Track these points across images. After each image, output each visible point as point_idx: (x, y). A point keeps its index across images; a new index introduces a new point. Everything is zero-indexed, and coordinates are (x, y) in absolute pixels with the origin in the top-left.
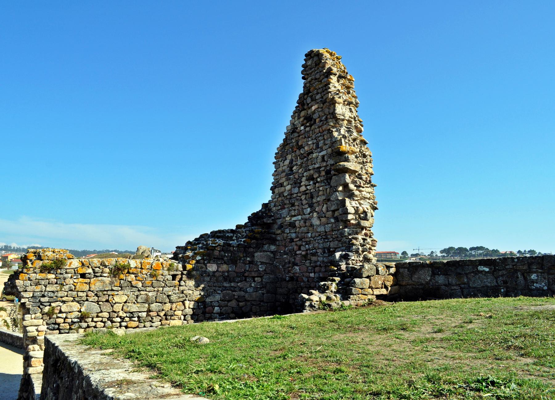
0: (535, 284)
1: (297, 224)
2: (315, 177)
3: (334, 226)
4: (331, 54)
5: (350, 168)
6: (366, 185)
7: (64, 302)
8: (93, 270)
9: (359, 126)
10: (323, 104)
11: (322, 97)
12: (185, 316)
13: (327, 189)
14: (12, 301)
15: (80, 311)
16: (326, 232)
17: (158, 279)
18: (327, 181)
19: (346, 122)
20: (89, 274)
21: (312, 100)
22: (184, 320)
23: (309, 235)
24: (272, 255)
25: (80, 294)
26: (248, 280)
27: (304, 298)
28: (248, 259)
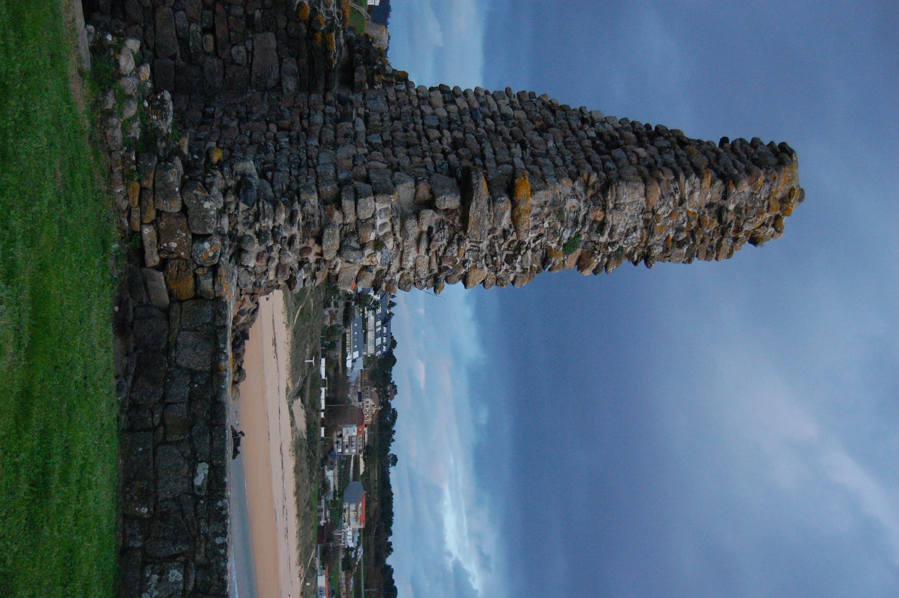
0: (156, 577)
5: (474, 204)
6: (434, 260)
9: (596, 262)
19: (599, 215)
24: (271, 83)
26: (206, 12)
28: (258, 14)
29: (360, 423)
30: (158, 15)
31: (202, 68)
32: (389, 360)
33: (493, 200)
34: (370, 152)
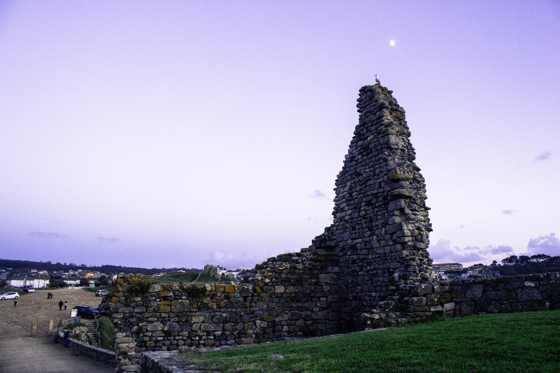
1: (358, 246)
2: (373, 202)
8: (174, 293)
11: (377, 129)
19: (399, 151)
20: (170, 296)
28: (313, 280)
30: (315, 318)
31: (332, 302)
33: (403, 187)
34: (376, 235)
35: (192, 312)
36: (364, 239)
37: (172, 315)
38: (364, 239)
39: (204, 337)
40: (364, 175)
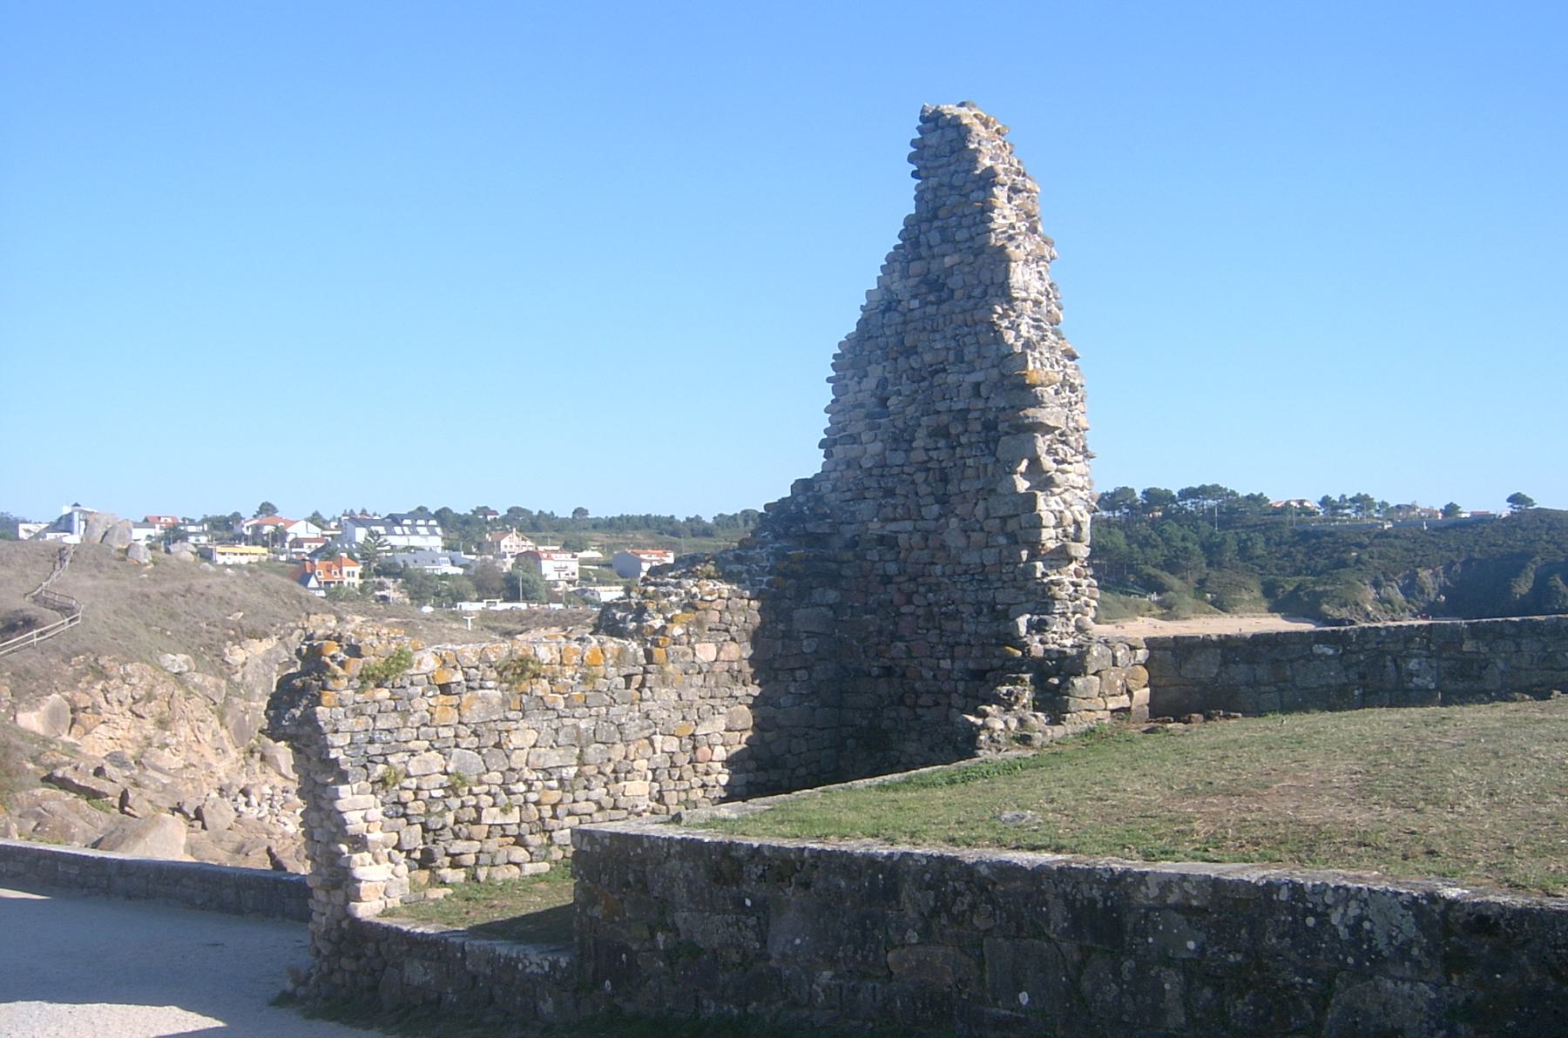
1: (902, 539)
2: (953, 431)
3: (1005, 553)
4: (986, 124)
7: (413, 753)
8: (465, 673)
9: (1055, 309)
10: (976, 256)
11: (972, 238)
12: (654, 771)
13: (986, 466)
14: (1490, 545)
15: (446, 773)
16: (984, 566)
17: (597, 687)
18: (988, 447)
19: (1030, 304)
20: (459, 683)
21: (944, 241)
22: (654, 780)
23: (938, 569)
25: (444, 732)
27: (973, 724)
29: (535, 556)
32: (443, 517)
35: (508, 720)
36: (920, 524)
37: (464, 731)
38: (920, 524)
39: (539, 784)
40: (928, 358)
